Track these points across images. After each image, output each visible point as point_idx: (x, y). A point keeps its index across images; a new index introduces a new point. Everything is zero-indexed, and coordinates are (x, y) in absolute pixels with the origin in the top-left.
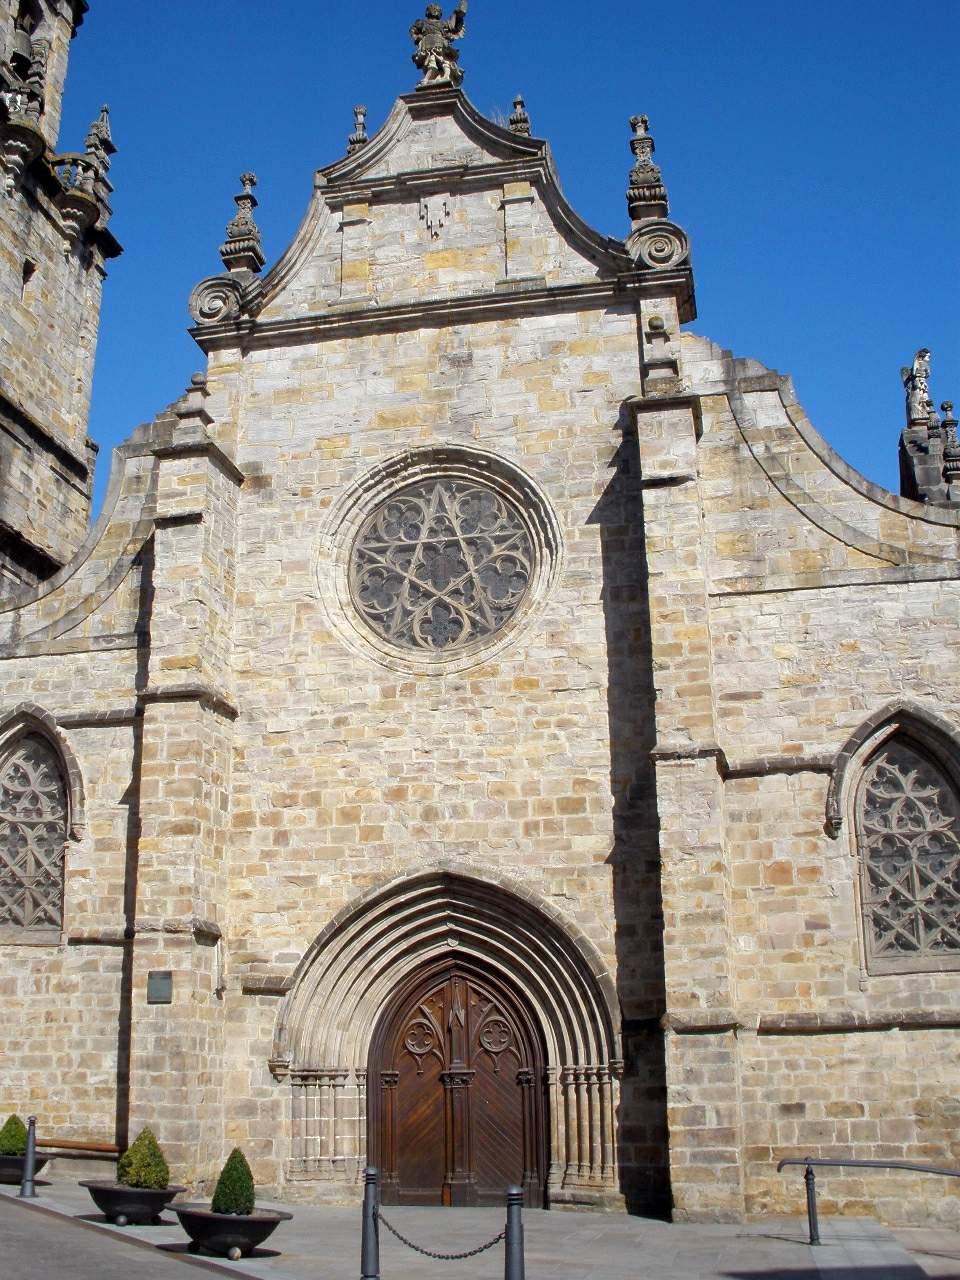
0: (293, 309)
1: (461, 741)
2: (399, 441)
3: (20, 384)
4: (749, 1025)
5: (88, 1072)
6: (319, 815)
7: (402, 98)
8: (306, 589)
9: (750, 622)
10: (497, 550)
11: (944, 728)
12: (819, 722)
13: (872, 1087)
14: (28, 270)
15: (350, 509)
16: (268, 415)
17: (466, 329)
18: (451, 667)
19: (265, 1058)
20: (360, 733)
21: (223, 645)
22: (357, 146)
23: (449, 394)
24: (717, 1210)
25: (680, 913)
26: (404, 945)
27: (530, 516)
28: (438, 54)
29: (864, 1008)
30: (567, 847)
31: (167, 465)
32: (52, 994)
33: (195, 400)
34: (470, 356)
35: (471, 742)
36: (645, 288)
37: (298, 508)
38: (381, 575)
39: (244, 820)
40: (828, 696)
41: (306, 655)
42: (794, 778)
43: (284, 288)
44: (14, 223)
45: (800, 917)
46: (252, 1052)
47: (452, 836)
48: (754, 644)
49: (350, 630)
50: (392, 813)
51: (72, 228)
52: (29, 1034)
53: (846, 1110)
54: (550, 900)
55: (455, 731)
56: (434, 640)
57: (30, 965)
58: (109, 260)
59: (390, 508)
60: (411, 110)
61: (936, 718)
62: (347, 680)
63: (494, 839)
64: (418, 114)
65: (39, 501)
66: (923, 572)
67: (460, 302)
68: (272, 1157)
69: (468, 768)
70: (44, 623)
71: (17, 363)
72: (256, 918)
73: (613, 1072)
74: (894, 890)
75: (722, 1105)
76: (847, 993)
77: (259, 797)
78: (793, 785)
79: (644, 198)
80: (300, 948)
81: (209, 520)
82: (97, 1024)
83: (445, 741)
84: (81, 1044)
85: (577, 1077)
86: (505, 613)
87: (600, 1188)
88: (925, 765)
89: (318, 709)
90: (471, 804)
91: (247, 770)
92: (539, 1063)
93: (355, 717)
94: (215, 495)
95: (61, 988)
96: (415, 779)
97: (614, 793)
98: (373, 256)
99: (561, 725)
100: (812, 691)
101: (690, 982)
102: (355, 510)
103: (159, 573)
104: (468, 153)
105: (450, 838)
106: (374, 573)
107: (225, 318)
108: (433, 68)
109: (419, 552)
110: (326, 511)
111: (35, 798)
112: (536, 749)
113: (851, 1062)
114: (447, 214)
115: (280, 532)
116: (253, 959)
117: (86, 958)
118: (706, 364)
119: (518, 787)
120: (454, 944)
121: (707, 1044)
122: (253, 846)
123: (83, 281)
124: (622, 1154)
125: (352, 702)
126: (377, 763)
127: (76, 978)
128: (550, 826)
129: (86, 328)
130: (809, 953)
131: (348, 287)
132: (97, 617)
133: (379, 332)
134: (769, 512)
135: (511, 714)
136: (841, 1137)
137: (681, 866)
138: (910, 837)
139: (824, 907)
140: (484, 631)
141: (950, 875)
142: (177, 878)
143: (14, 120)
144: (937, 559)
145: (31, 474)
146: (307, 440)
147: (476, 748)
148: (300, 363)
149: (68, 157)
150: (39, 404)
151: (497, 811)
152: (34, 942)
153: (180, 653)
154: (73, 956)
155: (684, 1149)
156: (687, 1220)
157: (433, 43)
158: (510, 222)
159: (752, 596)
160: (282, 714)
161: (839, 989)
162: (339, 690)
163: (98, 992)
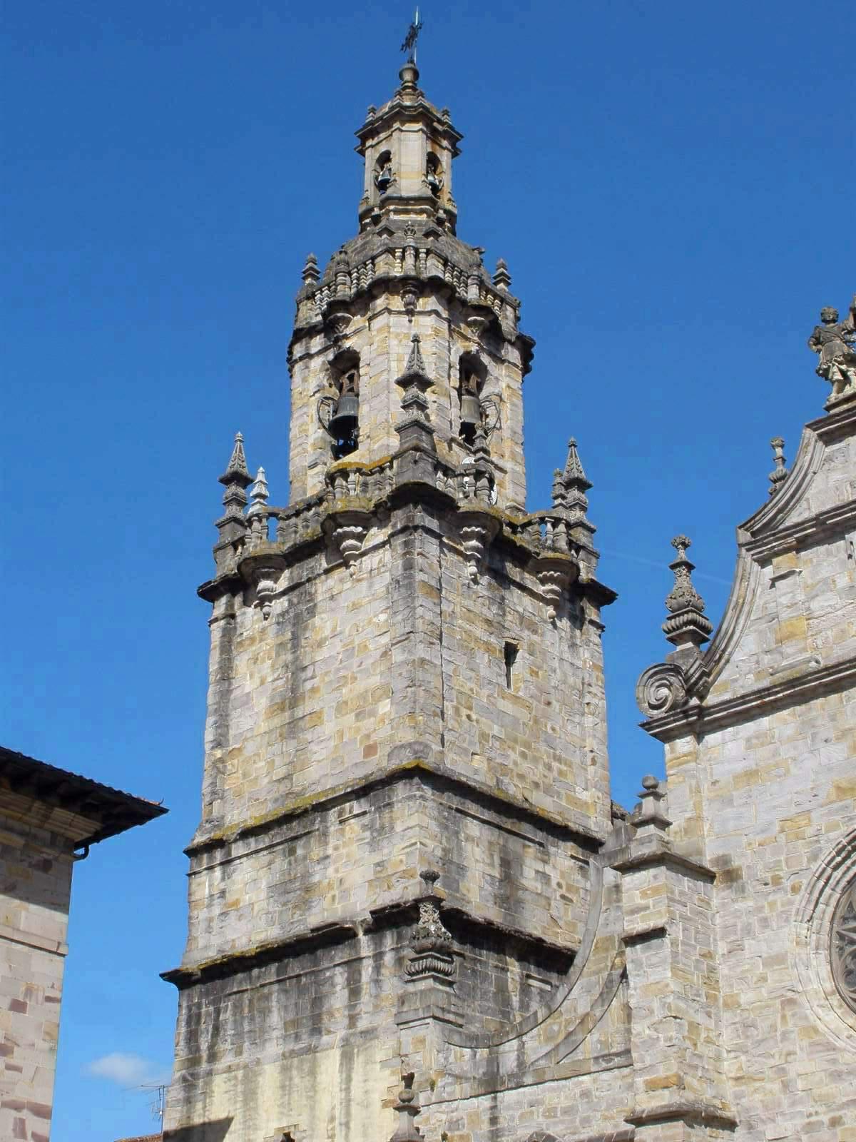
0: (740, 682)
3: (522, 777)
7: (808, 426)
8: (788, 984)
14: (510, 652)
21: (711, 1054)
22: (778, 484)
28: (841, 363)
31: (630, 880)
33: (649, 806)
37: (771, 898)
41: (795, 1053)
43: (728, 661)
44: (485, 610)
51: (552, 591)
58: (604, 608)
60: (820, 436)
62: (837, 1076)
64: (828, 439)
65: (563, 897)
70: (548, 1048)
71: (514, 756)
81: (676, 932)
89: (812, 1110)
94: (679, 902)
98: (809, 609)
102: (828, 891)
103: (633, 992)
107: (673, 707)
108: (838, 381)
110: (798, 897)
115: (756, 927)
123: (578, 642)
125: (844, 1100)
129: (589, 692)
131: (789, 649)
133: (825, 694)
143: (464, 505)
145: (548, 869)
146: (771, 823)
148: (754, 741)
149: (535, 516)
150: (548, 791)
153: (661, 1072)
157: (832, 353)
160: (779, 1118)
162: (831, 1088)
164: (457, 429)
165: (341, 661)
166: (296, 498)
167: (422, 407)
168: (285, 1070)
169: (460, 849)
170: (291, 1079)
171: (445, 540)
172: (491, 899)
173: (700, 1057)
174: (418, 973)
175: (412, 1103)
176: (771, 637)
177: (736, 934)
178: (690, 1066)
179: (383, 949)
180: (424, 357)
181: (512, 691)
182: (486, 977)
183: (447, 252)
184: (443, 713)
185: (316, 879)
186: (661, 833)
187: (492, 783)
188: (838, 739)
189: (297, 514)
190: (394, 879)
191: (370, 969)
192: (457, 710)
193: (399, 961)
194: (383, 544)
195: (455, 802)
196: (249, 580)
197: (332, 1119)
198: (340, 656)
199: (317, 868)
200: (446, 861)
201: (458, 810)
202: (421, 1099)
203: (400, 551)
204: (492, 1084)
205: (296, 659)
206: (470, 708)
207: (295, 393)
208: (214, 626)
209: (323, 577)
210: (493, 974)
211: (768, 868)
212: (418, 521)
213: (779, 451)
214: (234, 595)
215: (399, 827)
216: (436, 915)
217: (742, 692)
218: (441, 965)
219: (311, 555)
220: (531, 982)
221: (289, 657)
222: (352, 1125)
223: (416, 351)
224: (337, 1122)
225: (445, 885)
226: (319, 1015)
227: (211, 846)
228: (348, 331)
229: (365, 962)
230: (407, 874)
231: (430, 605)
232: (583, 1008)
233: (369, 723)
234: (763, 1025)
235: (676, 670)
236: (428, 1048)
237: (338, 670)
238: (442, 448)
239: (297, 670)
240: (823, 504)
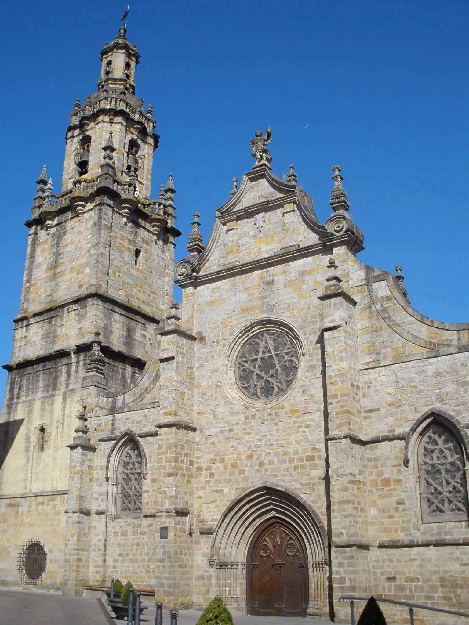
0: (212, 268)
2: (249, 318)
3: (138, 299)
4: (374, 544)
5: (150, 564)
6: (224, 466)
7: (245, 175)
9: (375, 379)
10: (286, 357)
11: (449, 418)
13: (422, 570)
14: (138, 253)
15: (234, 346)
16: (204, 312)
18: (269, 406)
19: (207, 558)
20: (237, 434)
25: (336, 501)
26: (256, 514)
28: (260, 152)
29: (419, 537)
30: (309, 475)
32: (139, 536)
34: (273, 280)
35: (275, 436)
36: (334, 244)
37: (215, 348)
39: (199, 469)
40: (405, 408)
43: (208, 260)
44: (129, 236)
45: (395, 499)
47: (269, 472)
48: (377, 389)
49: (235, 394)
50: (249, 464)
51: (156, 230)
52: (132, 551)
54: (302, 496)
55: (269, 431)
56: (265, 396)
57: (132, 525)
58: (177, 238)
60: (249, 178)
62: (233, 414)
63: (283, 473)
64: (252, 180)
66: (443, 352)
67: (267, 259)
69: (274, 446)
70: (133, 399)
71: (135, 291)
74: (435, 487)
75: (351, 576)
76: (413, 531)
77: (204, 462)
78: (391, 446)
79: (336, 203)
80: (218, 517)
81: (178, 358)
83: (266, 435)
84: (148, 554)
86: (289, 383)
89: (223, 426)
90: (275, 459)
93: (235, 428)
94: (181, 348)
96: (256, 451)
99: (307, 426)
100: (399, 406)
101: (340, 527)
102: (236, 346)
104: (271, 194)
106: (244, 370)
107: (187, 276)
109: (259, 361)
110: (225, 348)
111: (134, 464)
112: (298, 437)
113: (414, 560)
116: (203, 521)
117: (149, 522)
118: (359, 272)
119: (291, 452)
120: (274, 514)
121: (346, 552)
122: (203, 479)
126: (243, 445)
127: (146, 530)
128: (303, 467)
130: (397, 515)
131: (230, 257)
132: (149, 396)
133: (241, 274)
135: (289, 424)
138: (442, 464)
139: (403, 495)
140: (282, 390)
141: (458, 480)
142: (169, 492)
143: (123, 196)
144: (449, 345)
145: (146, 333)
148: (215, 290)
149: (152, 202)
150: (148, 304)
151: (284, 462)
153: (169, 409)
154: (145, 522)
155: (338, 594)
156: (339, 622)
157: (257, 148)
158: (286, 221)
159: (376, 369)
162: (231, 418)
164: (125, 167)
166: (64, 190)
167: (111, 158)
168: (43, 403)
169: (111, 324)
170: (45, 406)
171: (115, 209)
172: (122, 343)
173: (185, 405)
174: (90, 369)
175: (84, 417)
176: (224, 252)
178: (180, 408)
180: (114, 140)
181: (137, 267)
182: (117, 372)
183: (128, 101)
184: (108, 274)
186: (176, 322)
187: (126, 300)
189: (63, 196)
190: (85, 334)
192: (114, 273)
193: (85, 364)
194: (91, 210)
195: (110, 306)
196: (43, 220)
197: (58, 422)
200: (105, 328)
201: (111, 310)
202: (88, 415)
203: (97, 212)
205: (58, 251)
206: (120, 272)
207: (67, 150)
208: (30, 237)
210: (121, 371)
211: (215, 337)
212: (105, 201)
213: (235, 183)
214: (38, 225)
215: (88, 315)
216: (99, 348)
217: (212, 271)
218: (99, 366)
219: (66, 212)
220: (136, 374)
221: (55, 250)
223: (111, 137)
225: (104, 337)
226: (56, 383)
227: (23, 319)
228: (88, 128)
230: (89, 333)
231: (107, 233)
232: (146, 385)
234: (209, 394)
235: (189, 262)
236: (92, 396)
237: (72, 256)
238: (119, 174)
239: (57, 255)
240: (248, 204)
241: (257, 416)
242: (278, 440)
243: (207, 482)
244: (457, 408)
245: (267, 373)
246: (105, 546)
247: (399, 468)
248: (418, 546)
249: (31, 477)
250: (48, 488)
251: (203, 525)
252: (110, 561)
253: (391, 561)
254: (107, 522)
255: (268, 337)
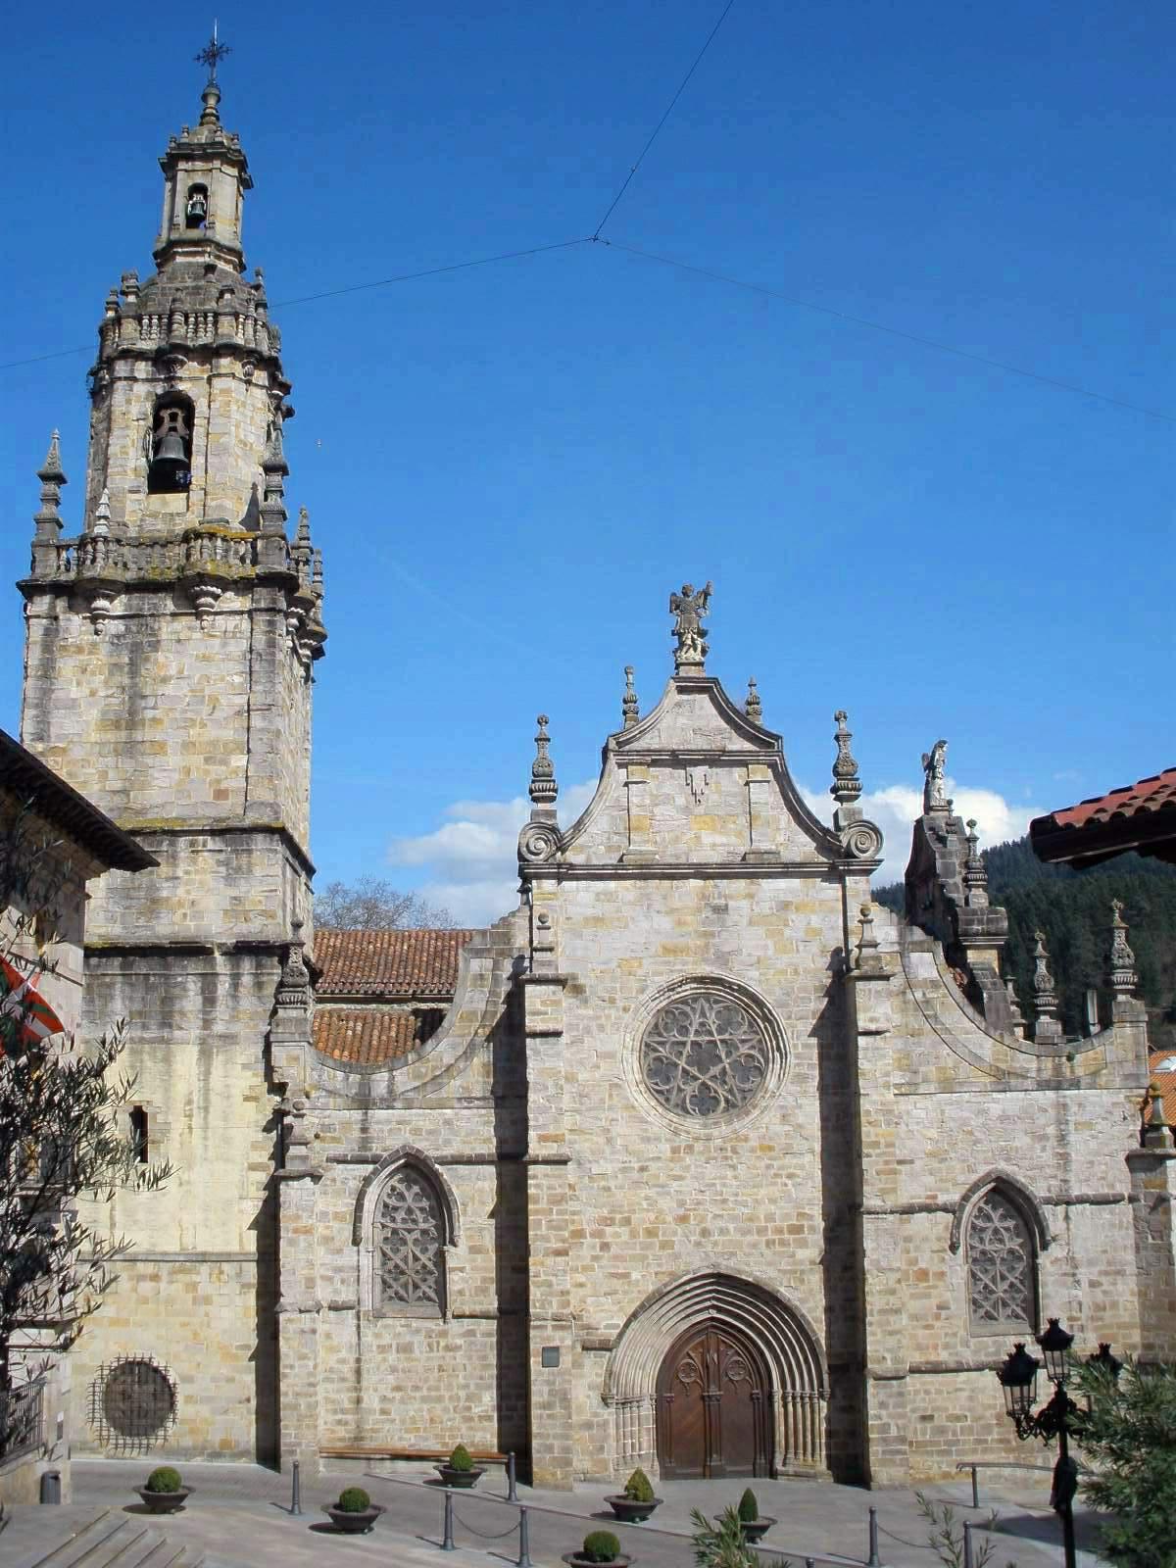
1: (724, 1185)
6: (631, 1231)
9: (908, 1113)
12: (947, 1181)
16: (581, 936)
17: (723, 884)
20: (657, 1177)
23: (712, 935)
24: (897, 1483)
25: (876, 1308)
27: (766, 1027)
29: (968, 1357)
30: (793, 1256)
32: (441, 1353)
34: (727, 905)
38: (662, 1062)
39: (579, 1234)
42: (931, 1216)
45: (934, 1302)
46: (590, 1389)
49: (643, 1101)
50: (679, 1231)
52: (426, 1380)
53: (958, 1418)
54: (782, 1290)
59: (667, 1012)
61: (1018, 1181)
62: (648, 1140)
63: (747, 1250)
64: (681, 690)
68: (605, 1456)
72: (589, 1300)
73: (821, 1396)
75: (900, 1422)
76: (959, 1348)
77: (588, 1216)
81: (565, 1039)
82: (478, 1373)
84: (467, 1386)
85: (794, 1398)
87: (812, 1467)
88: (1008, 1206)
90: (731, 1227)
91: (578, 1199)
92: (766, 1387)
95: (448, 1348)
96: (695, 1210)
97: (824, 1220)
98: (652, 812)
99: (790, 1176)
105: (719, 1249)
109: (688, 1047)
113: (961, 1390)
114: (707, 784)
115: (594, 1029)
116: (588, 1327)
117: (466, 1328)
119: (762, 1217)
120: (715, 1314)
121: (892, 1386)
124: (828, 1446)
127: (459, 1341)
128: (783, 1243)
130: (938, 1324)
134: (923, 1039)
136: (954, 1434)
137: (876, 1280)
140: (734, 1106)
147: (734, 1190)
148: (602, 897)
151: (746, 1232)
152: (419, 1315)
153: (551, 1131)
161: (955, 1347)
163: (477, 1351)
165: (188, 705)
177: (578, 1030)
179: (241, 971)
185: (164, 894)
188: (667, 913)
191: (227, 985)
197: (189, 1102)
198: (187, 699)
199: (165, 885)
204: (364, 1102)
209: (169, 618)
214: (57, 597)
215: (258, 871)
222: (211, 1110)
224: (195, 1105)
229: (221, 978)
232: (448, 1059)
233: (217, 770)
234: (595, 1098)
239: (136, 696)
241: (696, 1149)
242: (737, 1195)
243: (595, 1258)
244: (1029, 1173)
245: (703, 1070)
246: (358, 1372)
247: (942, 1254)
248: (969, 1370)
249: (112, 1217)
250: (173, 1247)
251: (587, 1334)
252: (371, 1401)
253: (927, 1392)
254: (358, 1327)
255: (706, 1006)
